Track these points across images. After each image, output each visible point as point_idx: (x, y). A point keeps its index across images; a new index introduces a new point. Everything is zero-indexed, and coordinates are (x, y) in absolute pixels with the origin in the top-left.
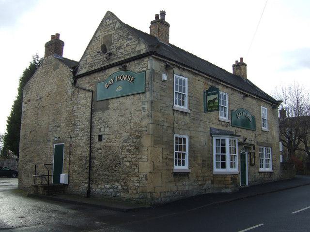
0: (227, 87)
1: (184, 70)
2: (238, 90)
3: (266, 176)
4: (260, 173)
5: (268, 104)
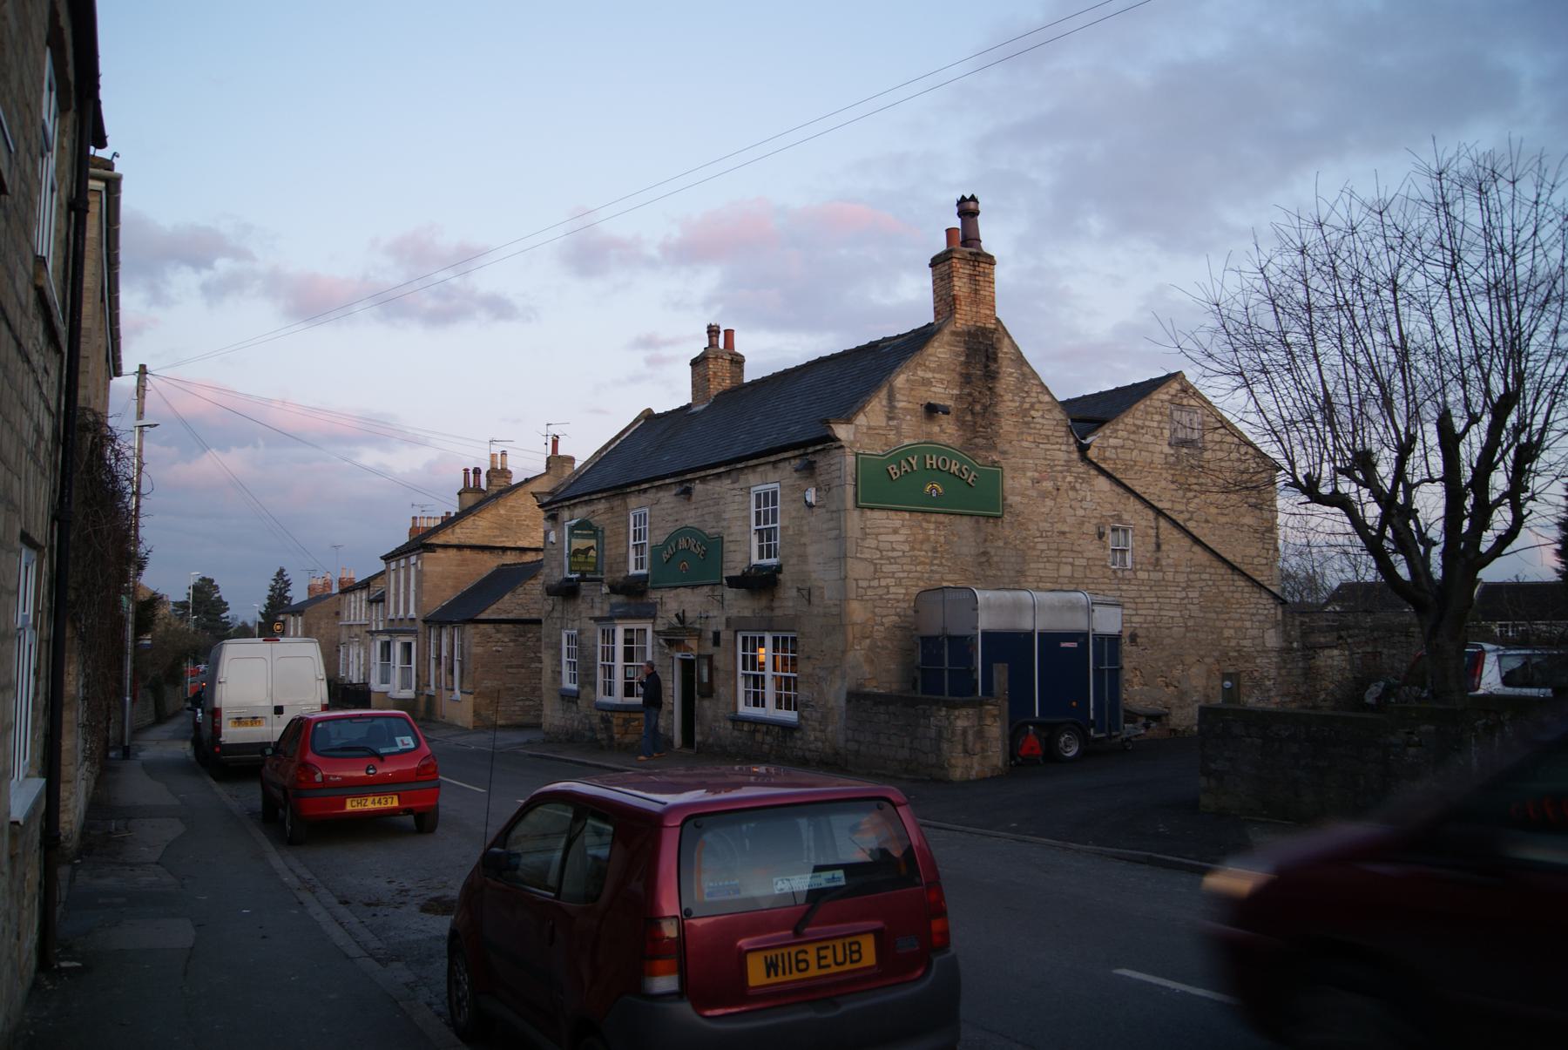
0: (645, 491)
1: (575, 505)
2: (667, 481)
3: (759, 737)
4: (737, 721)
5: (760, 469)
